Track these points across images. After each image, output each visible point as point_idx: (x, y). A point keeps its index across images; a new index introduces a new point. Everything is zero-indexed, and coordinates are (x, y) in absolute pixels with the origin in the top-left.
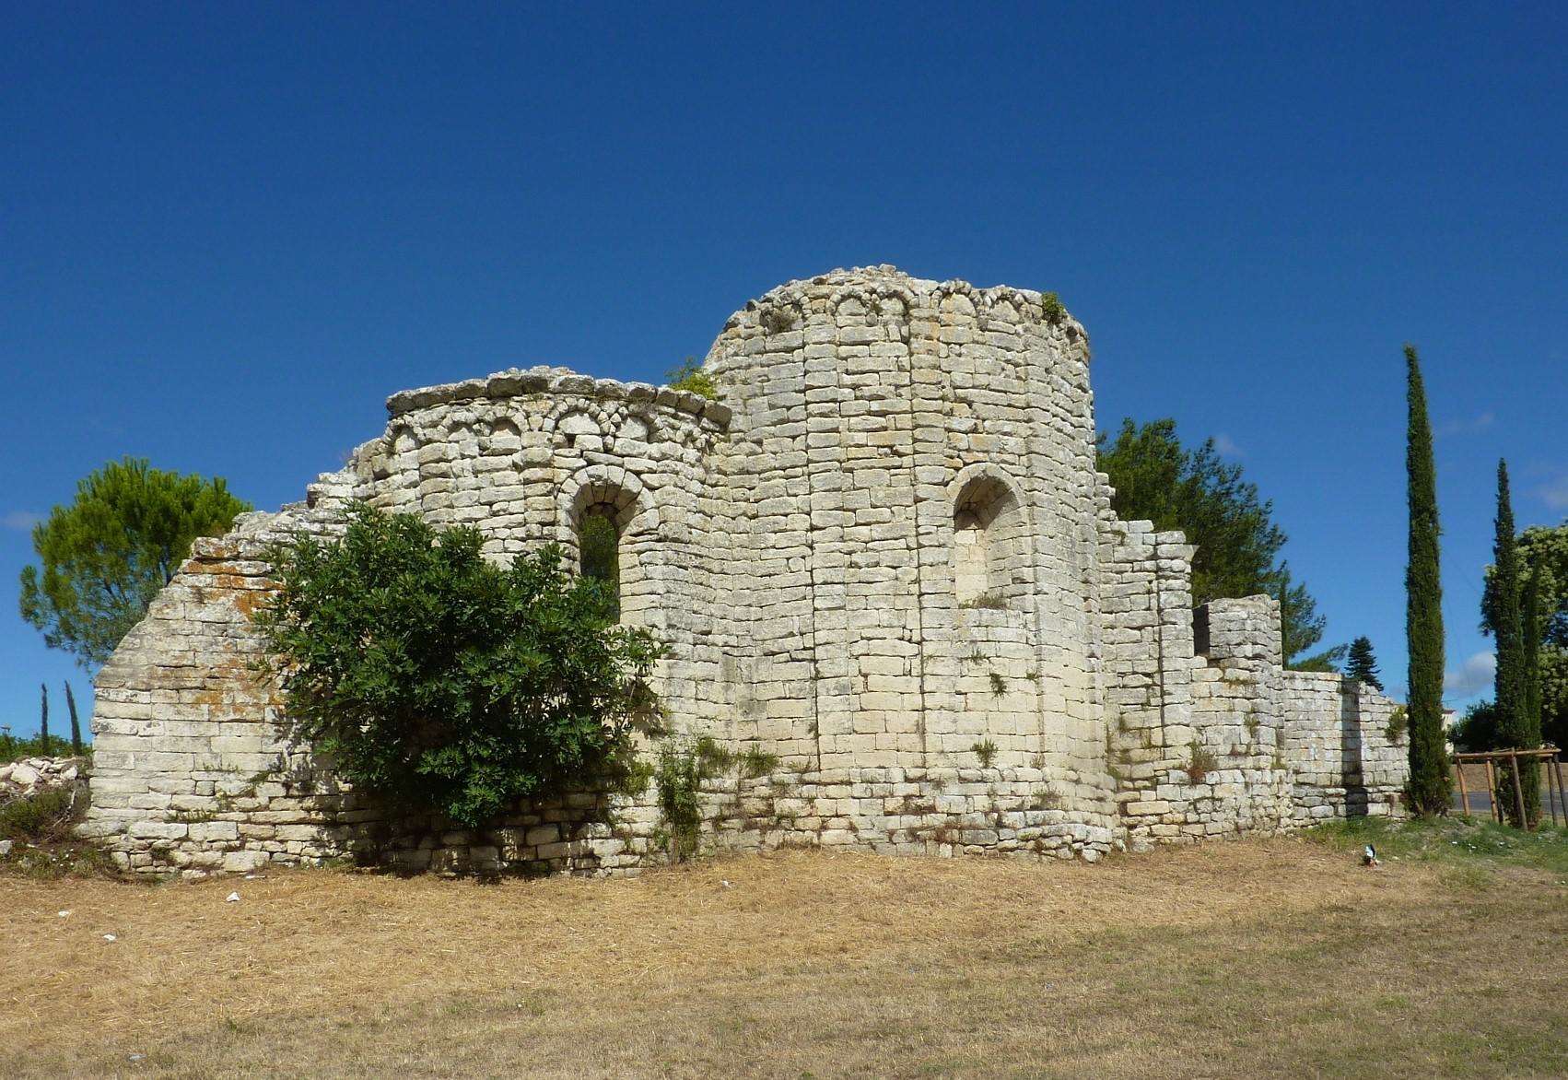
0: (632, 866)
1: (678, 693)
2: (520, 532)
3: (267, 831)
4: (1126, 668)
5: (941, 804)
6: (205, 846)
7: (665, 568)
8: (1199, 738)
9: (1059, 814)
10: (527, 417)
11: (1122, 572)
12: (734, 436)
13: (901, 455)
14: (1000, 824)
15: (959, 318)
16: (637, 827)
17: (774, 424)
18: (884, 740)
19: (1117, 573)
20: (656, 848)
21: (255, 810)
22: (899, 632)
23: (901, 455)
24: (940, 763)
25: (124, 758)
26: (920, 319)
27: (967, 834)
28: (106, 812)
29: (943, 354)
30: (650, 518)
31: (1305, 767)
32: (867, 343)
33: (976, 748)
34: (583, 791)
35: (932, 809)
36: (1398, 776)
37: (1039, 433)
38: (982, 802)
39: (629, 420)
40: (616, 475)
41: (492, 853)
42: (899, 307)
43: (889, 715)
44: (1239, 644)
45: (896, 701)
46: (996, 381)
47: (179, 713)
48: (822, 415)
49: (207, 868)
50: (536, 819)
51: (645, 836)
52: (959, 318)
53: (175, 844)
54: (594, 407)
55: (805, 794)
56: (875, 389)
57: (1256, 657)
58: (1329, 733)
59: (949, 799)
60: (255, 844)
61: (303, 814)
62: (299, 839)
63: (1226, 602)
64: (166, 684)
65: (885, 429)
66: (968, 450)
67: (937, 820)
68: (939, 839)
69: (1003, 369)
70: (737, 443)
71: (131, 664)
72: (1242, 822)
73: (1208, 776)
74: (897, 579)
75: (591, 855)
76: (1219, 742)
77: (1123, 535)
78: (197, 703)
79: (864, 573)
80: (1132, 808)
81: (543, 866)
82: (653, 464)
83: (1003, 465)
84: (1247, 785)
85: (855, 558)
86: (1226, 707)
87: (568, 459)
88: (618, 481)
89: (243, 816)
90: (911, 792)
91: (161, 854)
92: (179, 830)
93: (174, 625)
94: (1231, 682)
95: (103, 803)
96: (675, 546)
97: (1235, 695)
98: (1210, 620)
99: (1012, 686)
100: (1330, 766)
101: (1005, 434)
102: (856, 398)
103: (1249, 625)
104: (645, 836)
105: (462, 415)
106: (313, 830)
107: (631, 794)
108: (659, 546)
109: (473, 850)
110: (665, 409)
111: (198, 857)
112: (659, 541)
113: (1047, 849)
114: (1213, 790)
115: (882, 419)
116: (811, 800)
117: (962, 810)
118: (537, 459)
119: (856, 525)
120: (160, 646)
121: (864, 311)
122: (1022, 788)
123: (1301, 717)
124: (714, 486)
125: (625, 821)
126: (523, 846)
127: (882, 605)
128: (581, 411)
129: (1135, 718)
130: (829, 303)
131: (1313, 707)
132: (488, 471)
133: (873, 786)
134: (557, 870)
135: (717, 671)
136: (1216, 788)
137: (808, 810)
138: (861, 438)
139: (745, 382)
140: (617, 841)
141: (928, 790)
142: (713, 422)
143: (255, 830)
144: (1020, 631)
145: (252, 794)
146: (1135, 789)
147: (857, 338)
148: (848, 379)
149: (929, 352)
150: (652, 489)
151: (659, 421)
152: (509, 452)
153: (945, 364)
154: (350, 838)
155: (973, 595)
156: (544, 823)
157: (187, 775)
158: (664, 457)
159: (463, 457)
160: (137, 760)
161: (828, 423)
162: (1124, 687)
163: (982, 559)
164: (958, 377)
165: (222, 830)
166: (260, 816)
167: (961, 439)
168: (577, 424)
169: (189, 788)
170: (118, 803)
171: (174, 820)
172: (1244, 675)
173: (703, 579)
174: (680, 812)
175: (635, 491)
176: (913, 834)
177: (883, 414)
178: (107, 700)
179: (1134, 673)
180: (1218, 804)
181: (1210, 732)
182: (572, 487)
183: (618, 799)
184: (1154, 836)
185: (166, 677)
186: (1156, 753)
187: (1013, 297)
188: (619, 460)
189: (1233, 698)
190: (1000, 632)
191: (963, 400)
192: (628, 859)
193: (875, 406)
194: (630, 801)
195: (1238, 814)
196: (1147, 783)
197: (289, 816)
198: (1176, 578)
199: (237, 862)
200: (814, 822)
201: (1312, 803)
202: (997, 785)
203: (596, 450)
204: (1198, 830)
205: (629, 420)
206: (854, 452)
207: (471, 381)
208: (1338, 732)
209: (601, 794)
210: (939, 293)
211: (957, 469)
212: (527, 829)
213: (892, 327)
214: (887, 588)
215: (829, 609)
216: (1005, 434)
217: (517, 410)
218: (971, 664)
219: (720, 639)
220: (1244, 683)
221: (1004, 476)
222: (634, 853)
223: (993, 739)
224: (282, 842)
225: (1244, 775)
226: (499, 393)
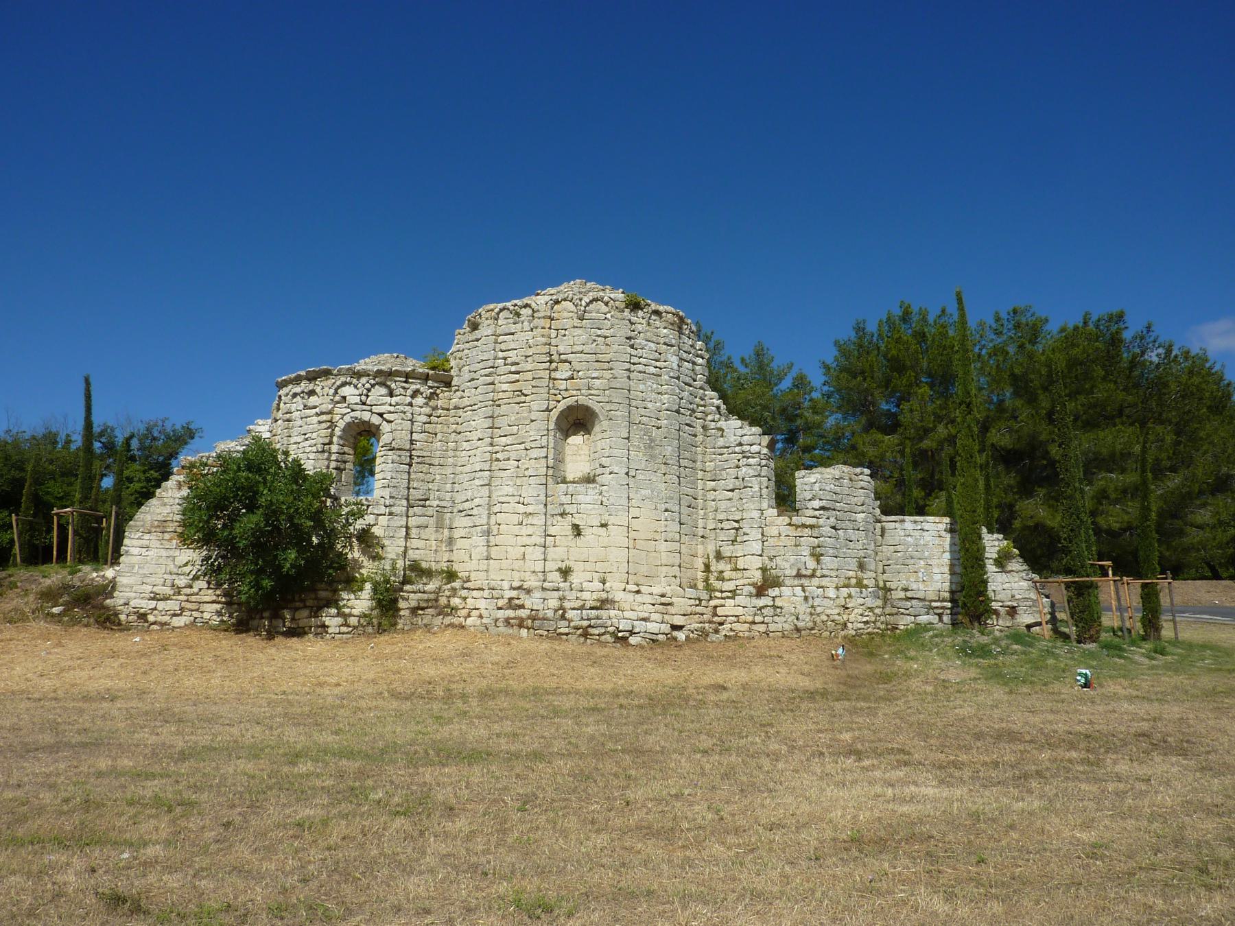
0: (347, 633)
1: (391, 535)
2: (314, 449)
3: (194, 606)
4: (722, 516)
5: (528, 604)
6: (163, 613)
7: (392, 465)
8: (769, 564)
9: (612, 613)
10: (323, 388)
11: (722, 454)
12: (454, 388)
13: (526, 395)
14: (563, 617)
15: (565, 314)
16: (355, 612)
17: (470, 381)
18: (505, 564)
19: (719, 455)
20: (365, 624)
21: (192, 595)
22: (517, 499)
23: (526, 395)
24: (532, 578)
25: (133, 567)
26: (539, 318)
27: (537, 623)
28: (121, 594)
29: (553, 336)
30: (385, 439)
31: (914, 586)
32: (513, 334)
33: (560, 570)
34: (327, 590)
35: (522, 607)
36: (1006, 594)
37: (617, 375)
38: (553, 603)
39: (377, 386)
40: (366, 416)
41: (280, 622)
42: (530, 312)
43: (509, 549)
44: (810, 500)
45: (512, 540)
46: (587, 348)
47: (162, 544)
48: (486, 375)
49: (163, 624)
50: (301, 605)
51: (357, 616)
52: (565, 314)
53: (149, 612)
54: (355, 381)
55: (463, 595)
56: (514, 359)
57: (822, 508)
58: (938, 561)
59: (533, 602)
60: (188, 613)
61: (214, 598)
62: (210, 612)
63: (803, 472)
64: (158, 530)
65: (518, 381)
66: (566, 390)
67: (523, 613)
68: (521, 626)
69: (595, 341)
70: (455, 392)
71: (143, 520)
72: (800, 624)
73: (770, 590)
74: (518, 467)
75: (324, 626)
76: (785, 566)
77: (723, 430)
78: (171, 539)
79: (502, 465)
80: (720, 611)
81: (301, 630)
82: (392, 409)
83: (590, 397)
84: (806, 598)
85: (498, 456)
86: (793, 543)
87: (341, 409)
88: (367, 419)
89: (185, 598)
90: (513, 596)
91: (143, 617)
92: (153, 604)
93: (166, 500)
94: (797, 527)
95: (121, 589)
96: (399, 452)
97: (800, 535)
98: (797, 483)
99: (586, 532)
100: (939, 586)
101: (593, 378)
102: (505, 365)
103: (817, 487)
104: (357, 616)
105: (298, 390)
106: (218, 606)
107: (354, 592)
108: (390, 453)
109: (273, 621)
110: (398, 379)
111: (160, 618)
112: (389, 450)
113: (591, 635)
114: (774, 600)
115: (518, 376)
116: (465, 599)
117: (540, 607)
118: (324, 411)
119: (500, 436)
120: (158, 511)
121: (511, 316)
122: (586, 595)
123: (910, 549)
124: (438, 417)
125: (348, 607)
126: (293, 619)
127: (510, 483)
128: (350, 384)
129: (727, 551)
130: (493, 314)
131: (922, 542)
132: (306, 417)
133: (493, 592)
134: (305, 633)
135: (432, 521)
136: (776, 599)
137: (463, 605)
138: (505, 387)
139: (461, 359)
140: (340, 619)
141: (523, 595)
142: (437, 382)
143: (189, 605)
144: (596, 497)
145: (191, 587)
146: (722, 598)
147: (508, 332)
148: (501, 354)
149: (543, 336)
150: (389, 422)
151: (393, 386)
152: (315, 407)
153: (553, 342)
154: (236, 612)
155: (579, 475)
156: (305, 607)
157: (161, 576)
158: (397, 404)
159: (297, 410)
160: (139, 568)
161: (489, 379)
162: (722, 529)
163: (587, 453)
164: (561, 349)
165: (172, 605)
166: (193, 598)
167: (561, 384)
168: (346, 391)
169: (161, 583)
170: (128, 590)
171: (152, 599)
172: (813, 521)
173: (424, 470)
174: (387, 604)
175: (377, 424)
176: (507, 621)
177: (518, 373)
178: (130, 538)
179: (728, 520)
180: (779, 610)
181: (779, 560)
182: (341, 424)
183: (344, 595)
184: (734, 631)
185: (159, 526)
186: (739, 574)
187: (603, 299)
188: (369, 408)
189: (800, 537)
190: (581, 498)
191: (566, 361)
192: (344, 629)
193: (513, 369)
194: (352, 596)
195: (797, 619)
196: (729, 594)
197: (207, 599)
198: (754, 458)
199: (179, 622)
200: (464, 613)
201: (917, 613)
202: (567, 593)
203: (356, 404)
204: (762, 628)
205: (377, 386)
206: (501, 395)
207: (299, 373)
208: (946, 560)
209: (336, 591)
210: (552, 302)
211: (559, 401)
212: (297, 609)
213: (526, 323)
214: (513, 473)
215: (481, 486)
216: (593, 378)
217: (318, 386)
218: (559, 518)
219: (435, 503)
220: (812, 527)
221: (590, 404)
222: (349, 626)
223: (571, 564)
224: (202, 612)
225: (804, 591)
226: (312, 378)
